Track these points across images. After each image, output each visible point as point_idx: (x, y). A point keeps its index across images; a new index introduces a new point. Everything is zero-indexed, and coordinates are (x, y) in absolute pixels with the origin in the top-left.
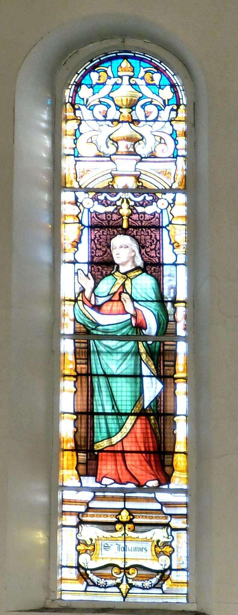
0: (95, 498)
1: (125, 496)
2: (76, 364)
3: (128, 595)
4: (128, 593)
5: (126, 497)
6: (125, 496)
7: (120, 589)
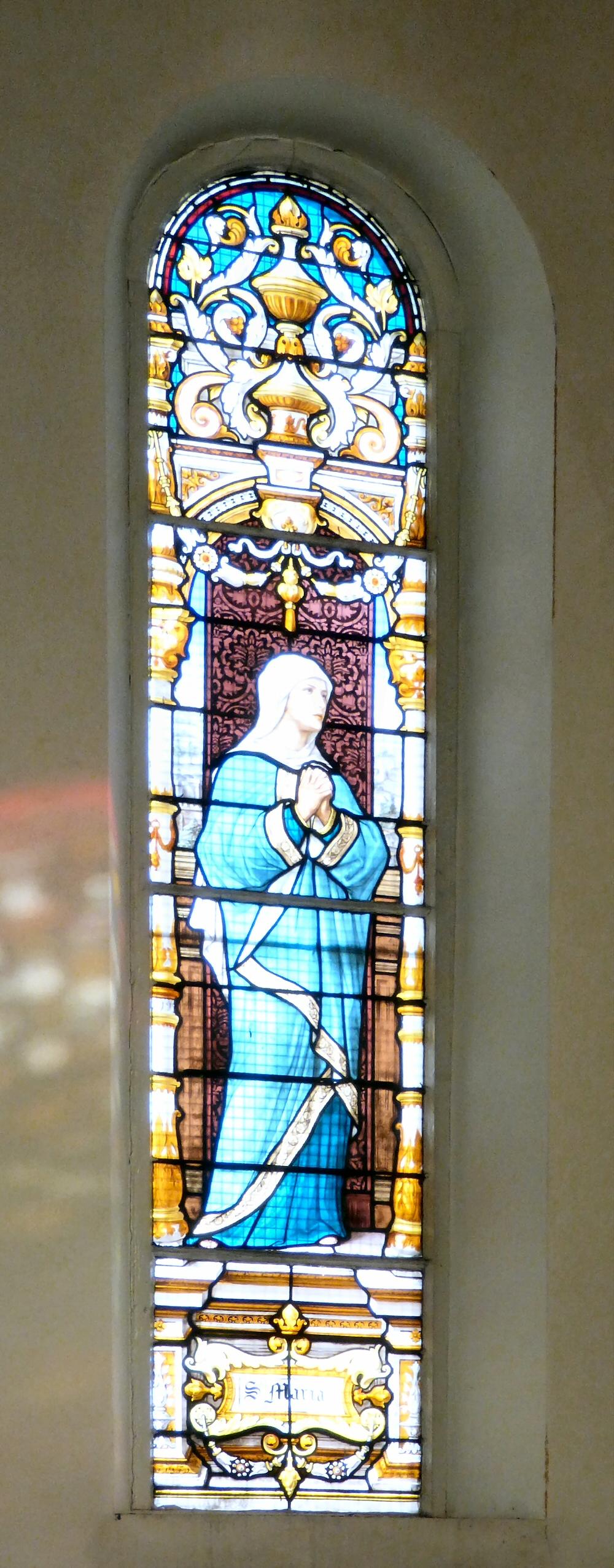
0: (225, 1276)
1: (291, 1274)
2: (180, 959)
3: (298, 1493)
4: (297, 1489)
5: (294, 1276)
6: (291, 1274)
7: (280, 1482)
